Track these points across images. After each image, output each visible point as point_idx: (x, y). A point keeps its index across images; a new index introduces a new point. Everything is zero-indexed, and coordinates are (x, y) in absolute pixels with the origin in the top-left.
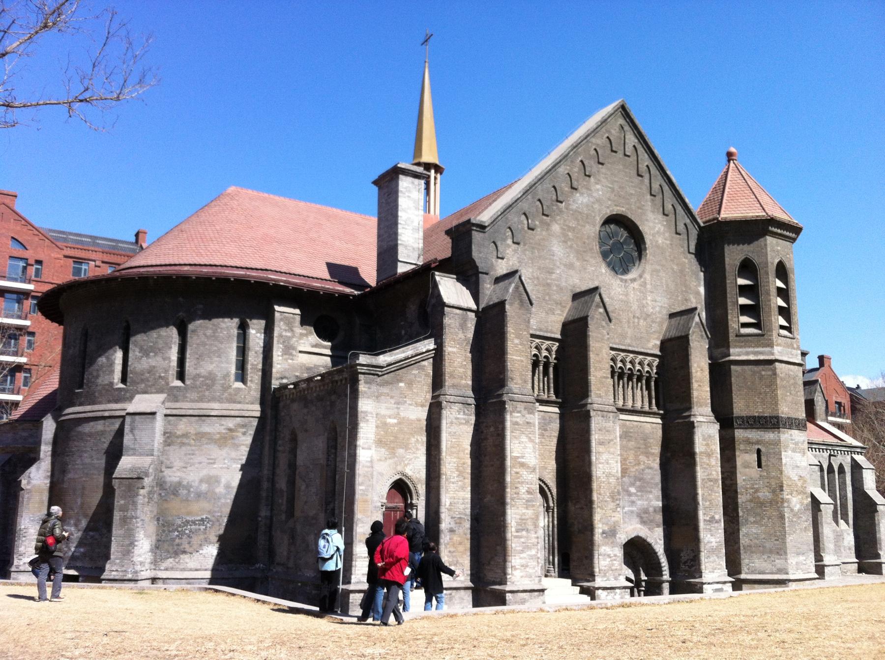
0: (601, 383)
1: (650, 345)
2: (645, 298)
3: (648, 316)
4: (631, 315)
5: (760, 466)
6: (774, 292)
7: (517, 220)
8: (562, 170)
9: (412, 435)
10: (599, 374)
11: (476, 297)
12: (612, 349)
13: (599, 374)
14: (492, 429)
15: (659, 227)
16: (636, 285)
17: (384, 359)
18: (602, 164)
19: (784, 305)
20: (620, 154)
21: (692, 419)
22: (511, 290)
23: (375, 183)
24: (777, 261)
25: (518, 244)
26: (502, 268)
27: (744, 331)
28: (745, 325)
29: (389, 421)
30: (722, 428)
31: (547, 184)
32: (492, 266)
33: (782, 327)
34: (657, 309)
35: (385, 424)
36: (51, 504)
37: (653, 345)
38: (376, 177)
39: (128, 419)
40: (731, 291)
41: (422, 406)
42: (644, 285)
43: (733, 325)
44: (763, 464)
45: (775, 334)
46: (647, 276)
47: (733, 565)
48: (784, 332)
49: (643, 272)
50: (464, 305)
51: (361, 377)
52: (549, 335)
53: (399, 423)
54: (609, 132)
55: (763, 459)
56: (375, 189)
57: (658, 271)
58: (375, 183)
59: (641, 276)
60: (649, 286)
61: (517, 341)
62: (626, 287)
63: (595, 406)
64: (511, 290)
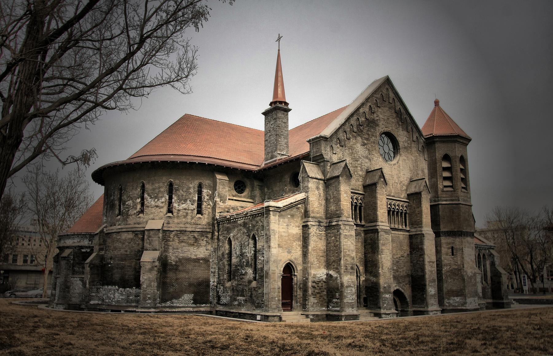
0: (383, 215)
1: (402, 196)
2: (400, 173)
3: (401, 182)
4: (394, 182)
5: (453, 255)
6: (459, 170)
7: (341, 135)
8: (361, 110)
9: (294, 241)
10: (382, 211)
11: (324, 173)
12: (352, 193)
13: (382, 211)
14: (333, 238)
15: (405, 139)
16: (396, 167)
17: (281, 204)
18: (379, 107)
19: (463, 177)
20: (387, 103)
21: (377, 227)
22: (10, 111)
23: (263, 114)
24: (460, 156)
25: (343, 146)
26: (335, 159)
27: (445, 189)
28: (445, 187)
29: (283, 234)
30: (436, 237)
31: (355, 117)
32: (331, 158)
33: (463, 188)
34: (405, 178)
35: (282, 236)
36: (4, 270)
37: (403, 196)
38: (264, 111)
39: (146, 233)
40: (439, 170)
41: (299, 227)
42: (399, 167)
43: (440, 186)
44: (455, 253)
45: (459, 191)
46: (400, 162)
47: (441, 303)
48: (464, 190)
49: (399, 160)
50: (319, 177)
51: (271, 213)
52: (357, 192)
53: (288, 236)
54: (382, 91)
55: (454, 251)
56: (263, 117)
57: (405, 160)
58: (263, 114)
59: (398, 163)
60: (401, 167)
61: (345, 195)
62: (391, 168)
63: (381, 227)
64: (10, 111)
